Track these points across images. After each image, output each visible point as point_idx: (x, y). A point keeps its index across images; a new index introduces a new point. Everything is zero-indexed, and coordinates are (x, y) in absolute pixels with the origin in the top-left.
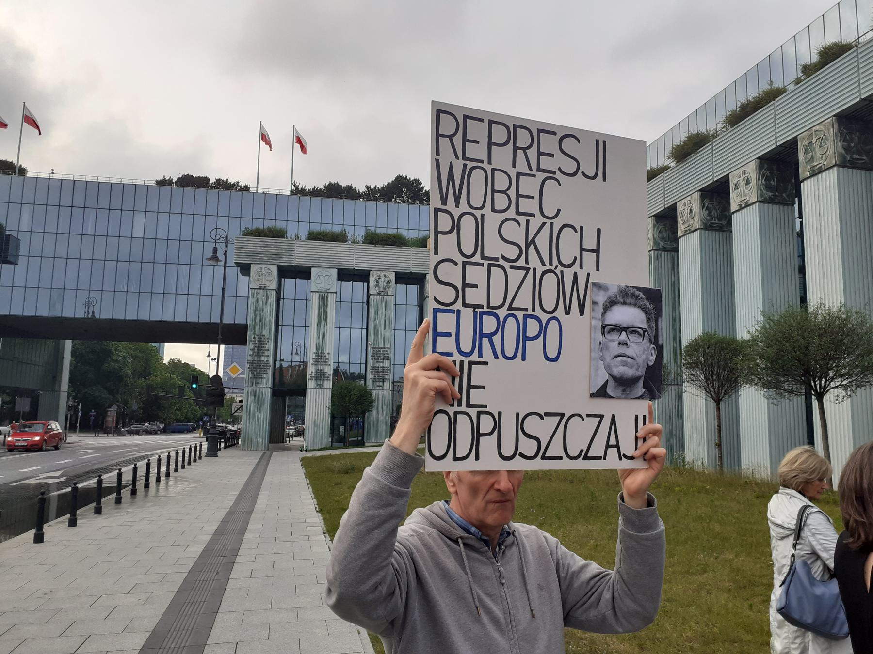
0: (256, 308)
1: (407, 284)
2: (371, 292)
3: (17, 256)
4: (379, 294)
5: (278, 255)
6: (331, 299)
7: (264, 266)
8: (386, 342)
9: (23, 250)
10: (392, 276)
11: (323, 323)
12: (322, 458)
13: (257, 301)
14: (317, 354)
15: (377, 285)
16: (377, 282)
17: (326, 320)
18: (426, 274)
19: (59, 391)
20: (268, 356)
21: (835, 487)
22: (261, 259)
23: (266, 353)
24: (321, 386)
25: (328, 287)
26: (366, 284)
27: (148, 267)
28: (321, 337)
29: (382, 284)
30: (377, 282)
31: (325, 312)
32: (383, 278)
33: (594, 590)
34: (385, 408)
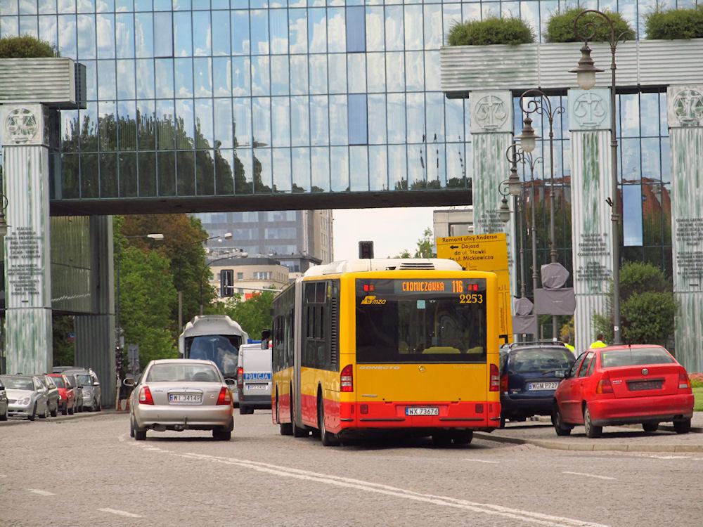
4: (684, 126)
7: (490, 94)
11: (592, 184)
13: (483, 154)
14: (586, 236)
16: (680, 105)
17: (596, 178)
21: (149, 236)
22: (485, 83)
25: (597, 120)
28: (591, 208)
30: (680, 105)
31: (595, 165)
32: (689, 97)
33: (22, 97)
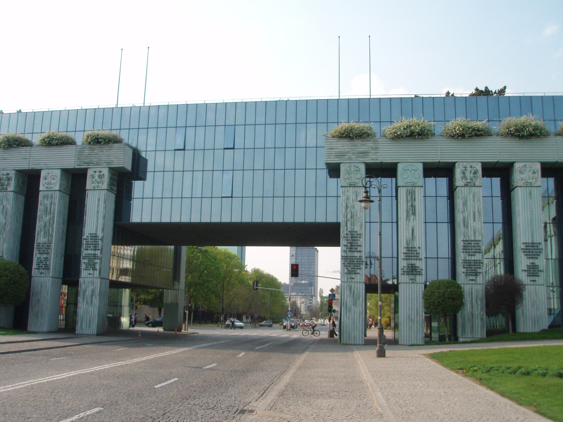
0: (347, 207)
1: (436, 176)
2: (399, 185)
3: (145, 172)
4: (466, 185)
5: (365, 153)
6: (419, 193)
7: (352, 165)
8: (477, 234)
9: (150, 167)
10: (479, 167)
12: (472, 353)
13: (348, 199)
15: (464, 177)
16: (464, 173)
17: (414, 214)
18: (455, 163)
19: (121, 306)
20: (360, 251)
22: (350, 158)
23: (359, 249)
24: (413, 281)
26: (394, 179)
27: (248, 174)
29: (468, 175)
30: (464, 173)
31: (413, 206)
32: (469, 169)
34: (479, 302)
